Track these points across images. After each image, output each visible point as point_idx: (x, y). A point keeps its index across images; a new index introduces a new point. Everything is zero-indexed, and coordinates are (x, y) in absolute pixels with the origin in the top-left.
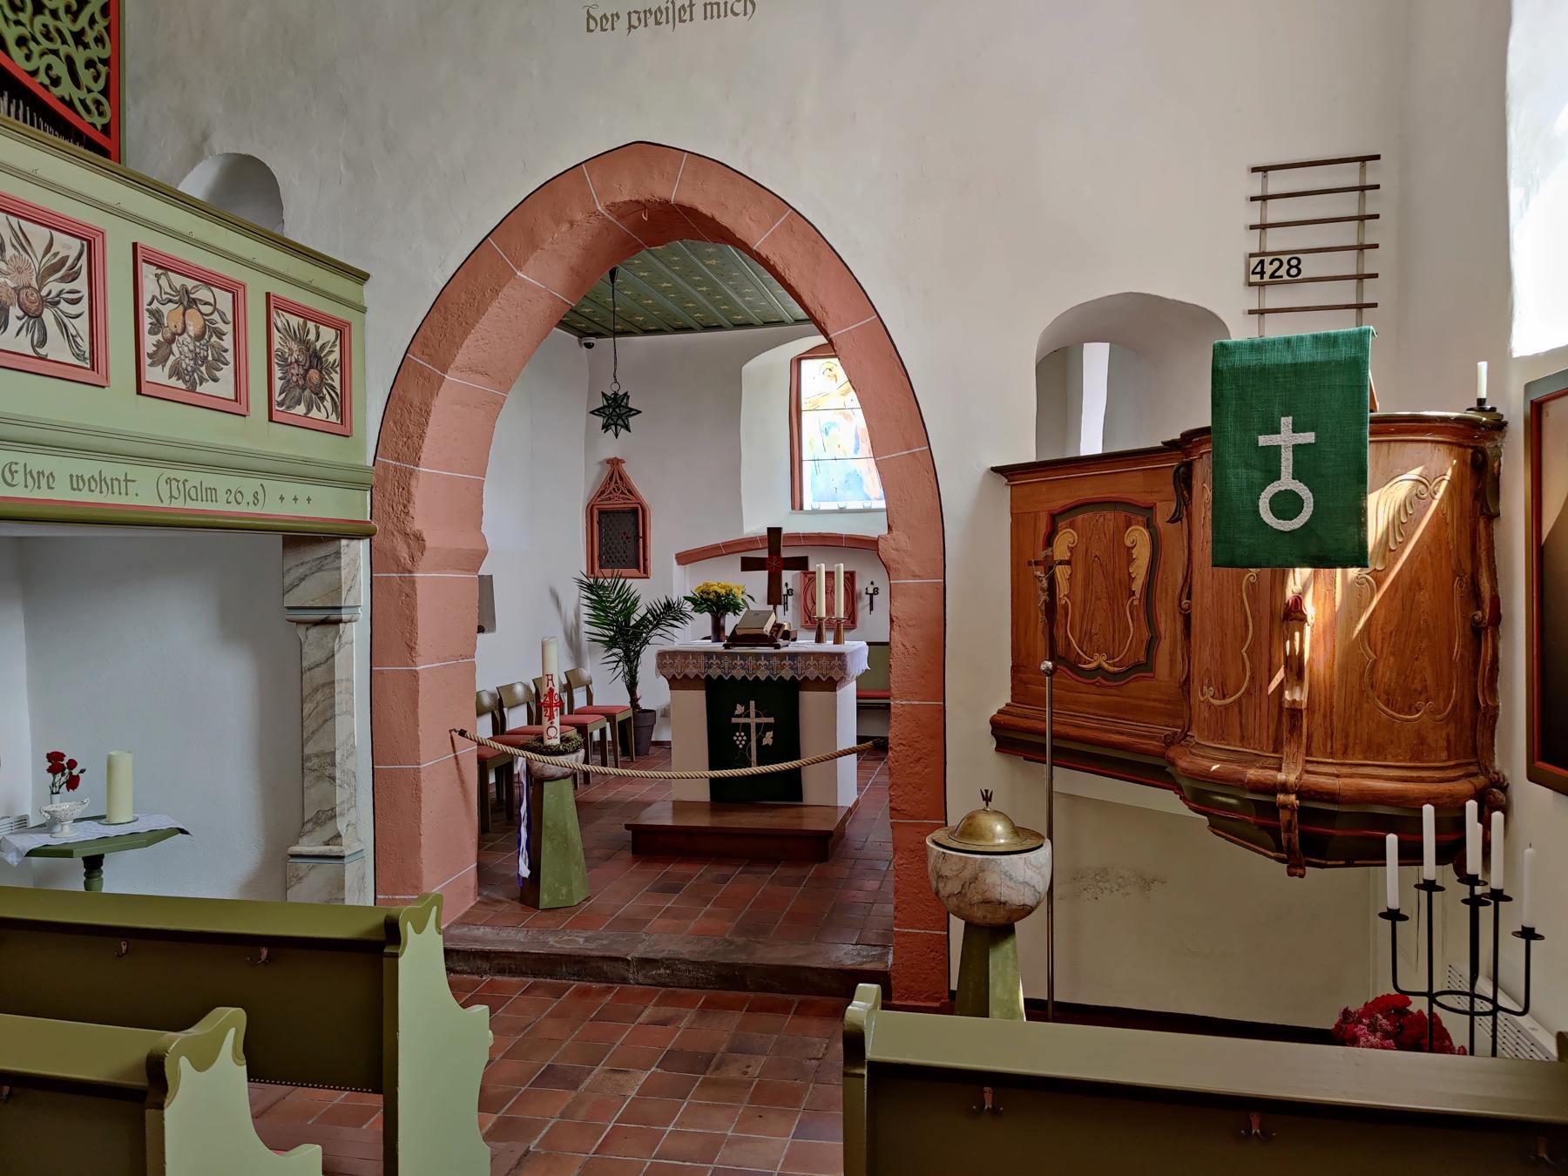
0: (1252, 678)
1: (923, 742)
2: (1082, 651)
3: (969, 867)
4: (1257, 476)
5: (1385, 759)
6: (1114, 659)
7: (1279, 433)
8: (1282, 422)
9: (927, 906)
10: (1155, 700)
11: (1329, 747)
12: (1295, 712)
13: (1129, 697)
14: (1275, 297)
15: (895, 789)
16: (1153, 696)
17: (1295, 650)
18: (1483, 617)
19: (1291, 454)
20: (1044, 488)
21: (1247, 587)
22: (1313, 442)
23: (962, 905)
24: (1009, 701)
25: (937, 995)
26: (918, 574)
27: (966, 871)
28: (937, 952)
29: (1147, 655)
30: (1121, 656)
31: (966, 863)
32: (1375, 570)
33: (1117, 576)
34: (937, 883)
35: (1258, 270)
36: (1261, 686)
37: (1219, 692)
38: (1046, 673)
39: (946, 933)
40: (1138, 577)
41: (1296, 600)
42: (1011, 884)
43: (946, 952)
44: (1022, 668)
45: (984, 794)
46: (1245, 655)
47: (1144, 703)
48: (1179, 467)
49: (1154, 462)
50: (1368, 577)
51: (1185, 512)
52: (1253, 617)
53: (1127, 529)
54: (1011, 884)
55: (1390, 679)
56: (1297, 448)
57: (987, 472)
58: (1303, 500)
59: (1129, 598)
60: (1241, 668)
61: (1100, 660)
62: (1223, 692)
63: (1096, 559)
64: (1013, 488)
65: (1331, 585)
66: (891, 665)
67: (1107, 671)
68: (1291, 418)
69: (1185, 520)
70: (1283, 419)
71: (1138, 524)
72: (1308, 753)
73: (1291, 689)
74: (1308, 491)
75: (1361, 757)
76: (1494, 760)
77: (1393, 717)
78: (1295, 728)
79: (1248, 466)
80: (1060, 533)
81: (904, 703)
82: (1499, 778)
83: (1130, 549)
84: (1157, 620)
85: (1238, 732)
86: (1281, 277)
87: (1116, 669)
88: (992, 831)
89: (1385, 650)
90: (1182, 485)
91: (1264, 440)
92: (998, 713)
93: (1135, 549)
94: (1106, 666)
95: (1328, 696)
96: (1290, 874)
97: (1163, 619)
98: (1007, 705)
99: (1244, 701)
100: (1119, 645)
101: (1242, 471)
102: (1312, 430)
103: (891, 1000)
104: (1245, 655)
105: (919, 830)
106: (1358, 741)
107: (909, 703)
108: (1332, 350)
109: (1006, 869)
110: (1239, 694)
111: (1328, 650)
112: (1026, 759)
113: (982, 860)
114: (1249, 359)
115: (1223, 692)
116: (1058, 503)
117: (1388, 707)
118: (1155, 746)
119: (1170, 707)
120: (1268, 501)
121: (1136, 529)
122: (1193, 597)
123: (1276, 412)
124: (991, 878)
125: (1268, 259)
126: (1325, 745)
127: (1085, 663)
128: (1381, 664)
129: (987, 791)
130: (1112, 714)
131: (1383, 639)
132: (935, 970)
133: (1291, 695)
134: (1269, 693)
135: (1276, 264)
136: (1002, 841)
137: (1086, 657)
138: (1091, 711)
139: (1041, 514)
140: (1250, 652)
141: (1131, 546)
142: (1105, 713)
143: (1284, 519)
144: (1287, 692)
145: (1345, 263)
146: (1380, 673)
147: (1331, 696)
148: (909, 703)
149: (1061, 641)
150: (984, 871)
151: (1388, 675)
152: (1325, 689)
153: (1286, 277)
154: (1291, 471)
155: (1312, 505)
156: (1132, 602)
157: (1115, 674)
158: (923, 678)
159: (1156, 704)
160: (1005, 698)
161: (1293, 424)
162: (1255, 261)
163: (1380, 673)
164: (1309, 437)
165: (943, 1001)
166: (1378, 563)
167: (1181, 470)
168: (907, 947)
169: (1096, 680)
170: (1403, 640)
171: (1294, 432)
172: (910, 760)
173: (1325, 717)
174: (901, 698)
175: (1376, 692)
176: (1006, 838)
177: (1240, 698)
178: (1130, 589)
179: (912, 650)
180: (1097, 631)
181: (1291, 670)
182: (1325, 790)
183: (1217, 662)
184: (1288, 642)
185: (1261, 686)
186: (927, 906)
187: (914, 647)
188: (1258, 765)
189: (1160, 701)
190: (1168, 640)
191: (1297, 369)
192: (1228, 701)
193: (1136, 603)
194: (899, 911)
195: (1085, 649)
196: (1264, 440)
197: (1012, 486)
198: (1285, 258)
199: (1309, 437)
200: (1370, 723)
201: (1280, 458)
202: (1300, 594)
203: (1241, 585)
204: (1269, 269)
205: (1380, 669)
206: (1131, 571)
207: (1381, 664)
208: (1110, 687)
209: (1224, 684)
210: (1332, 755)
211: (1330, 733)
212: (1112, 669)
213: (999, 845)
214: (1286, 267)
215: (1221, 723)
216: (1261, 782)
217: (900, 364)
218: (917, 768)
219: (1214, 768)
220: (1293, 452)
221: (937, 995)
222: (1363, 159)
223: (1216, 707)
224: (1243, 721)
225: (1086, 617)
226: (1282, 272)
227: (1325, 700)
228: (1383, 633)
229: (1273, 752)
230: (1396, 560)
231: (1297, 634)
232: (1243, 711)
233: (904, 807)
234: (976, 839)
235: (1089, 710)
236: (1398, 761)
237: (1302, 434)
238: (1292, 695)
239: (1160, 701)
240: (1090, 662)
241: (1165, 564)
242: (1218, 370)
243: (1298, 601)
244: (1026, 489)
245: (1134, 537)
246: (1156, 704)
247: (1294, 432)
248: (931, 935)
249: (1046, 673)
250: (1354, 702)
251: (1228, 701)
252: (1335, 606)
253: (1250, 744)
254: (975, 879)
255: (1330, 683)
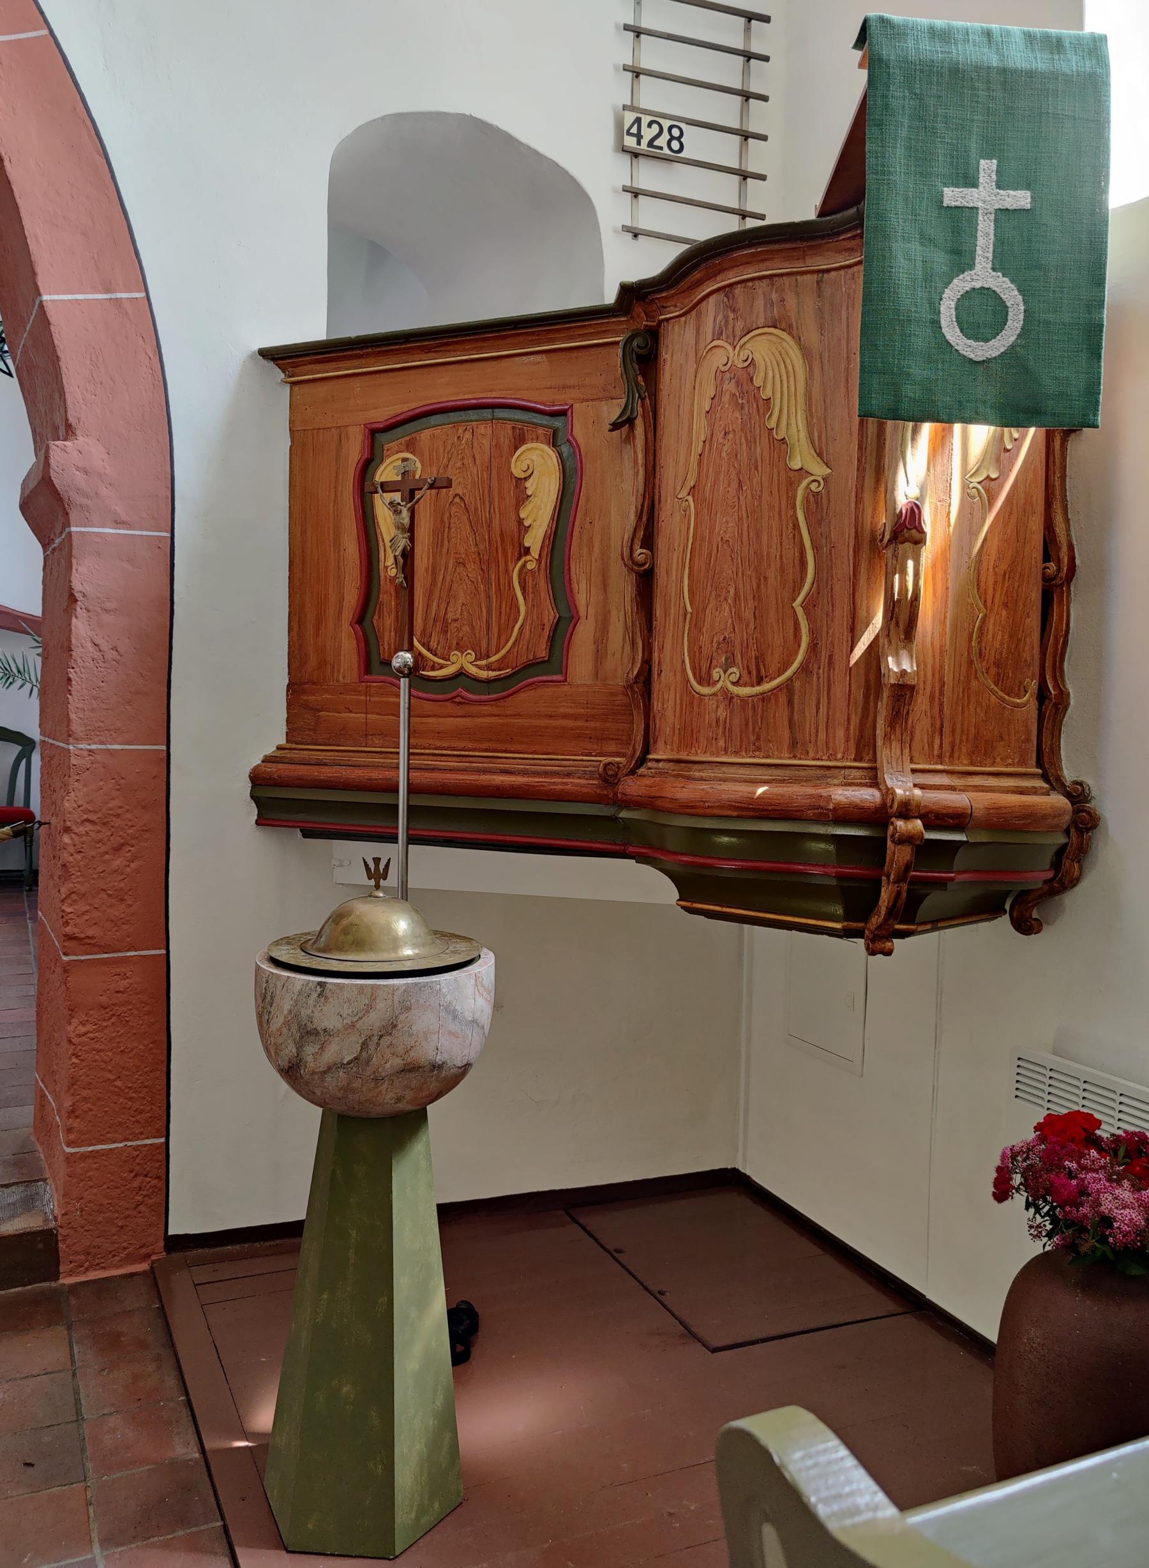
0: (813, 647)
1: (129, 816)
2: (429, 650)
3: (380, 1005)
4: (940, 260)
5: (993, 764)
6: (488, 657)
7: (975, 185)
8: (981, 167)
9: (131, 1099)
10: (566, 716)
11: (936, 746)
12: (904, 691)
13: (519, 715)
14: (650, 176)
15: (75, 901)
16: (562, 710)
17: (907, 590)
18: (1059, 570)
19: (992, 224)
20: (357, 385)
21: (806, 499)
22: (1028, 206)
23: (356, 1084)
24: (282, 741)
25: (143, 1251)
26: (124, 518)
27: (373, 1014)
28: (146, 1176)
29: (551, 646)
30: (503, 652)
31: (373, 998)
32: (988, 477)
33: (496, 524)
34: (300, 1048)
35: (634, 130)
36: (831, 657)
37: (749, 673)
38: (401, 672)
39: (163, 1140)
40: (535, 525)
41: (912, 509)
42: (453, 1027)
43: (163, 1171)
44: (306, 686)
45: (372, 866)
46: (800, 612)
47: (543, 722)
48: (629, 341)
49: (572, 338)
50: (979, 486)
51: (640, 409)
52: (816, 548)
53: (516, 448)
54: (453, 1027)
55: (1002, 644)
56: (1003, 215)
57: (252, 356)
58: (1007, 307)
59: (519, 559)
60: (792, 631)
61: (463, 661)
62: (758, 670)
63: (457, 499)
64: (296, 388)
65: (945, 493)
66: (69, 680)
67: (476, 680)
68: (995, 161)
69: (639, 425)
70: (982, 162)
71: (537, 439)
72: (912, 761)
73: (897, 655)
74: (1016, 293)
75: (965, 762)
76: (1061, 769)
77: (1004, 700)
78: (897, 717)
79: (926, 240)
80: (388, 461)
81: (94, 747)
82: (1083, 790)
83: (520, 482)
84: (571, 590)
85: (786, 734)
86: (661, 148)
87: (492, 674)
88: (388, 929)
89: (997, 601)
90: (636, 366)
91: (952, 196)
92: (263, 762)
93: (531, 481)
94: (473, 670)
95: (937, 666)
96: (873, 953)
97: (583, 586)
98: (279, 748)
99: (797, 684)
100: (499, 637)
101: (915, 248)
102: (1028, 188)
103: (56, 1278)
104: (800, 612)
105: (118, 970)
106: (965, 737)
107: (103, 747)
108: (1056, 57)
109: (448, 998)
110: (789, 673)
111: (939, 593)
112: (308, 834)
113: (407, 990)
114: (928, 49)
115: (758, 670)
116: (382, 414)
117: (997, 685)
118: (582, 786)
119: (592, 724)
120: (953, 305)
121: (535, 449)
122: (661, 543)
123: (974, 146)
124: (422, 1021)
125: (646, 120)
126: (931, 744)
127: (433, 669)
128: (992, 620)
129: (377, 861)
130: (485, 745)
131: (995, 582)
132: (142, 1208)
133: (899, 664)
134: (852, 662)
135: (655, 129)
136: (408, 952)
137: (436, 659)
138: (445, 744)
139: (351, 430)
140: (810, 606)
141: (523, 476)
142: (470, 745)
143: (977, 339)
144: (890, 659)
145: (725, 150)
146: (990, 636)
147: (942, 667)
148: (103, 747)
149: (386, 634)
150: (408, 1009)
151: (999, 637)
152: (934, 656)
153: (666, 151)
154: (990, 255)
155: (1022, 316)
156: (524, 566)
157: (488, 681)
158: (129, 703)
159: (570, 723)
160: (273, 735)
161: (999, 172)
162: (630, 117)
163: (990, 636)
164: (1021, 199)
165: (154, 1257)
166: (991, 469)
167: (635, 343)
168: (90, 1179)
169: (454, 694)
170: (1016, 584)
171: (999, 187)
172: (103, 849)
173: (932, 698)
174: (89, 739)
175: (984, 664)
176: (414, 946)
177: (790, 679)
178: (521, 544)
179: (111, 654)
180: (458, 616)
181: (897, 624)
182: (951, 811)
183: (747, 626)
184: (897, 576)
185: (831, 657)
186: (131, 1099)
187: (115, 648)
188: (836, 781)
189: (575, 717)
190: (591, 619)
191: (1007, 78)
192: (766, 686)
193: (530, 566)
194: (77, 1117)
195: (433, 644)
196: (952, 196)
197: (293, 383)
198: (666, 124)
199: (1021, 199)
200: (978, 710)
201: (977, 230)
202: (917, 499)
203: (795, 497)
204: (648, 133)
205: (991, 627)
206: (522, 516)
207: (992, 620)
208: (480, 702)
209: (760, 659)
210: (940, 759)
211: (938, 723)
212: (484, 674)
213: (409, 959)
214: (666, 136)
215: (755, 723)
216: (856, 806)
217: (93, 132)
218: (118, 862)
219: (760, 790)
220: (996, 220)
221: (143, 1251)
222: (750, 17)
223: (744, 700)
224: (796, 717)
225: (436, 596)
226: (662, 141)
227: (933, 675)
228: (996, 574)
229: (855, 760)
230: (1012, 464)
231: (910, 564)
232: (796, 701)
233: (90, 932)
234: (371, 950)
235: (438, 744)
236: (1007, 766)
237: (1012, 192)
238: (898, 663)
239: (575, 717)
240: (442, 667)
241: (588, 500)
242: (880, 60)
243: (914, 512)
244: (322, 390)
245: (529, 462)
246: (570, 723)
247: (999, 187)
248: (136, 1148)
249: (401, 672)
250: (962, 678)
251: (766, 686)
252: (949, 525)
253: (807, 752)
254: (391, 1027)
255: (941, 646)
